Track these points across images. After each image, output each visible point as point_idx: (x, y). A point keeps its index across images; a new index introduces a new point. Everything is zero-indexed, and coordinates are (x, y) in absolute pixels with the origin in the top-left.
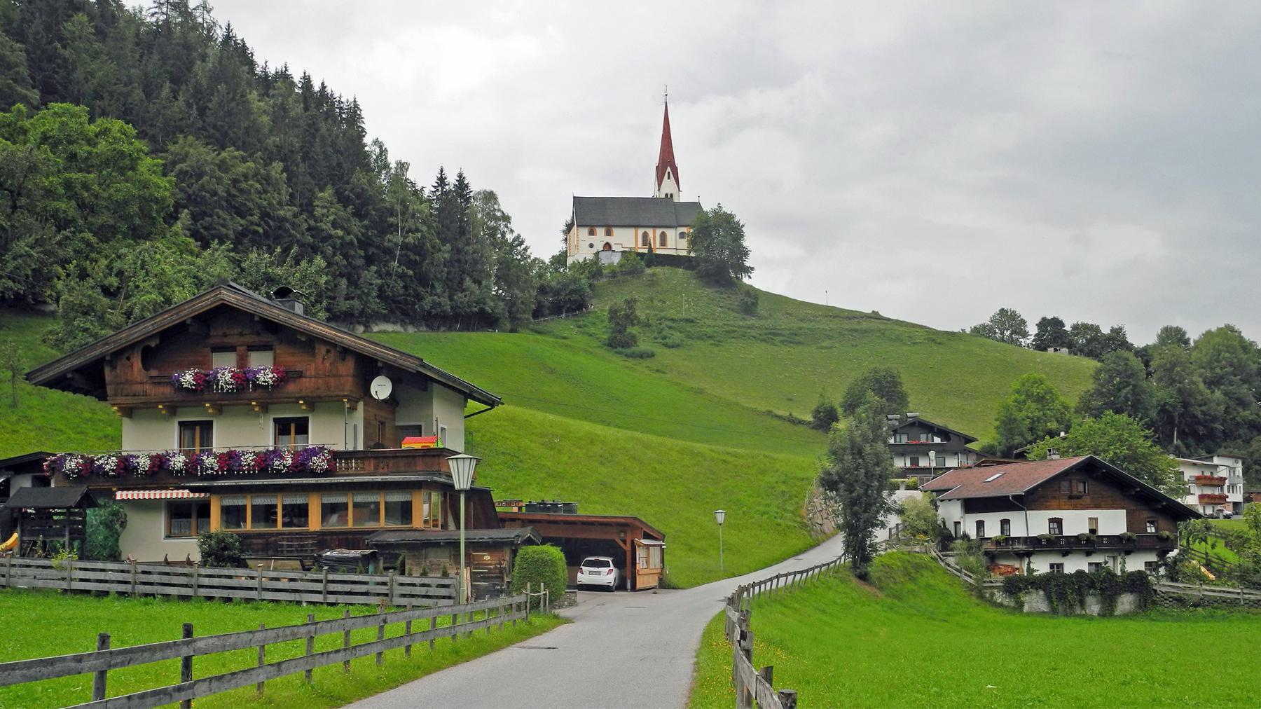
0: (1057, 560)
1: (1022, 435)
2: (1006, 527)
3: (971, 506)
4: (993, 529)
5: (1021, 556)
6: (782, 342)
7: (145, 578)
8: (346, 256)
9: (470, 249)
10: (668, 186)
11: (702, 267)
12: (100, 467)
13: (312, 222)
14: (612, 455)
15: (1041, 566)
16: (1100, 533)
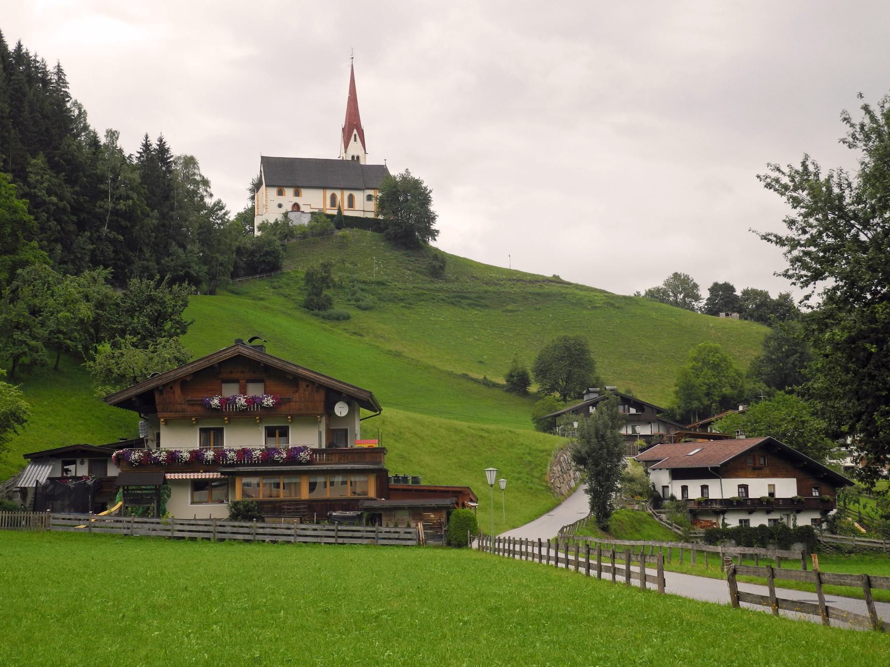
0: (744, 517)
1: (699, 399)
2: (705, 491)
3: (677, 474)
4: (695, 493)
5: (717, 513)
6: (469, 305)
7: (221, 529)
8: (59, 221)
9: (174, 213)
10: (355, 148)
11: (391, 230)
12: (156, 458)
13: (26, 189)
14: (400, 433)
15: (733, 521)
16: (777, 496)
